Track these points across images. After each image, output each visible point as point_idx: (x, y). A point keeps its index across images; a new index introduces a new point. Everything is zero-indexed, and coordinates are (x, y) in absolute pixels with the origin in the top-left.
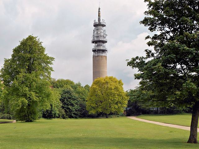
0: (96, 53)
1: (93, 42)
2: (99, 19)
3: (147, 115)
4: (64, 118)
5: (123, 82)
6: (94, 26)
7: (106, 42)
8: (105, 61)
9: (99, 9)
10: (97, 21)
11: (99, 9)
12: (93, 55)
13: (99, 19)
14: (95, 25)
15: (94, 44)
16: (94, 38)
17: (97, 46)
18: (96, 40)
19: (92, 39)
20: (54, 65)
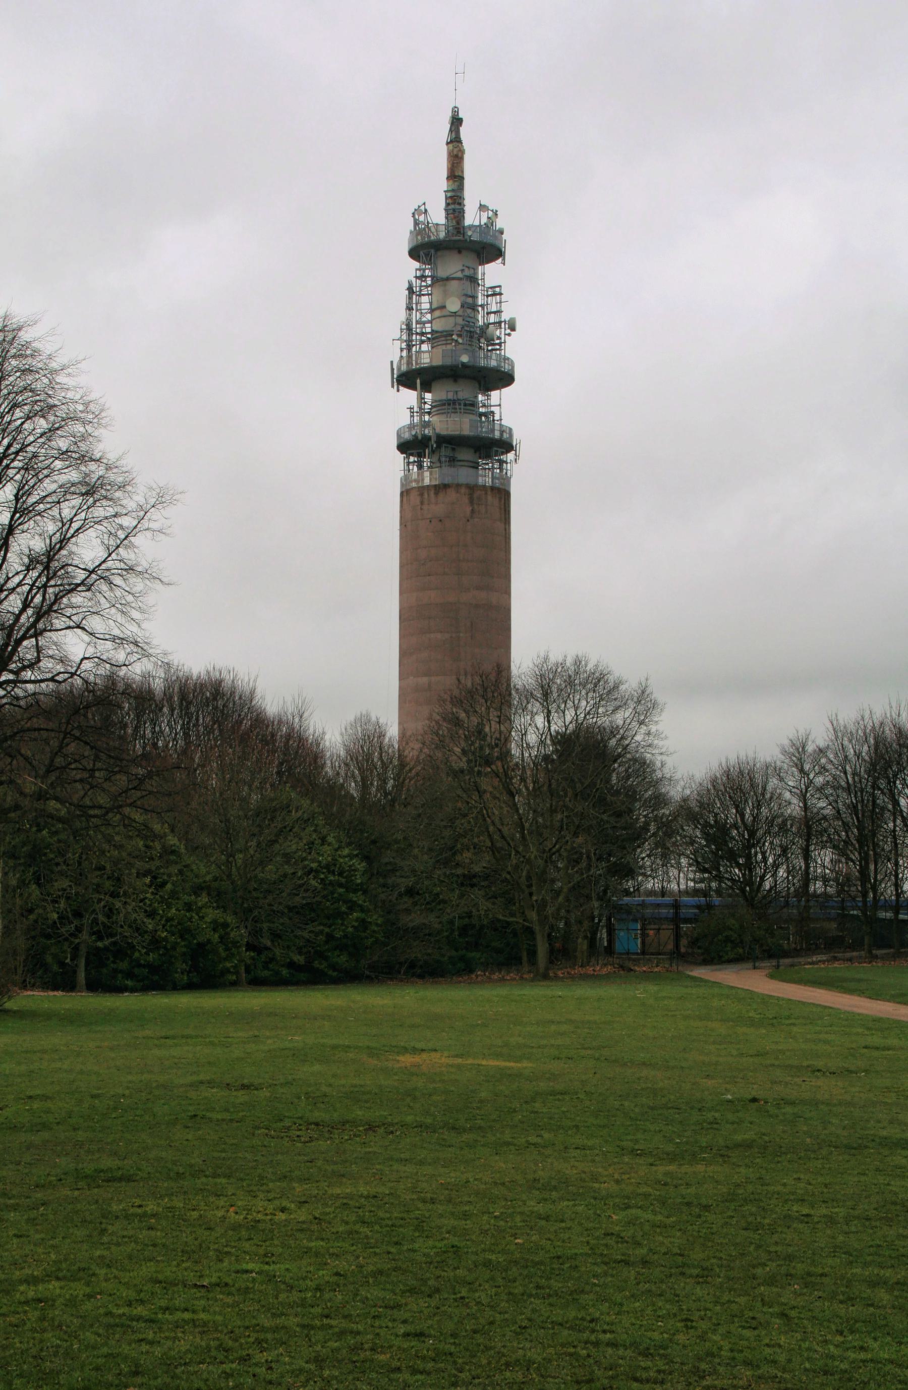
0: (426, 462)
1: (405, 379)
2: (455, 202)
3: (718, 967)
4: (402, 494)
5: (658, 695)
6: (414, 253)
7: (504, 378)
8: (500, 525)
9: (456, 122)
10: (438, 216)
11: (456, 122)
12: (405, 480)
13: (455, 202)
14: (424, 249)
15: (410, 397)
16: (409, 347)
17: (441, 406)
18: (426, 360)
19: (391, 353)
20: (156, 597)
